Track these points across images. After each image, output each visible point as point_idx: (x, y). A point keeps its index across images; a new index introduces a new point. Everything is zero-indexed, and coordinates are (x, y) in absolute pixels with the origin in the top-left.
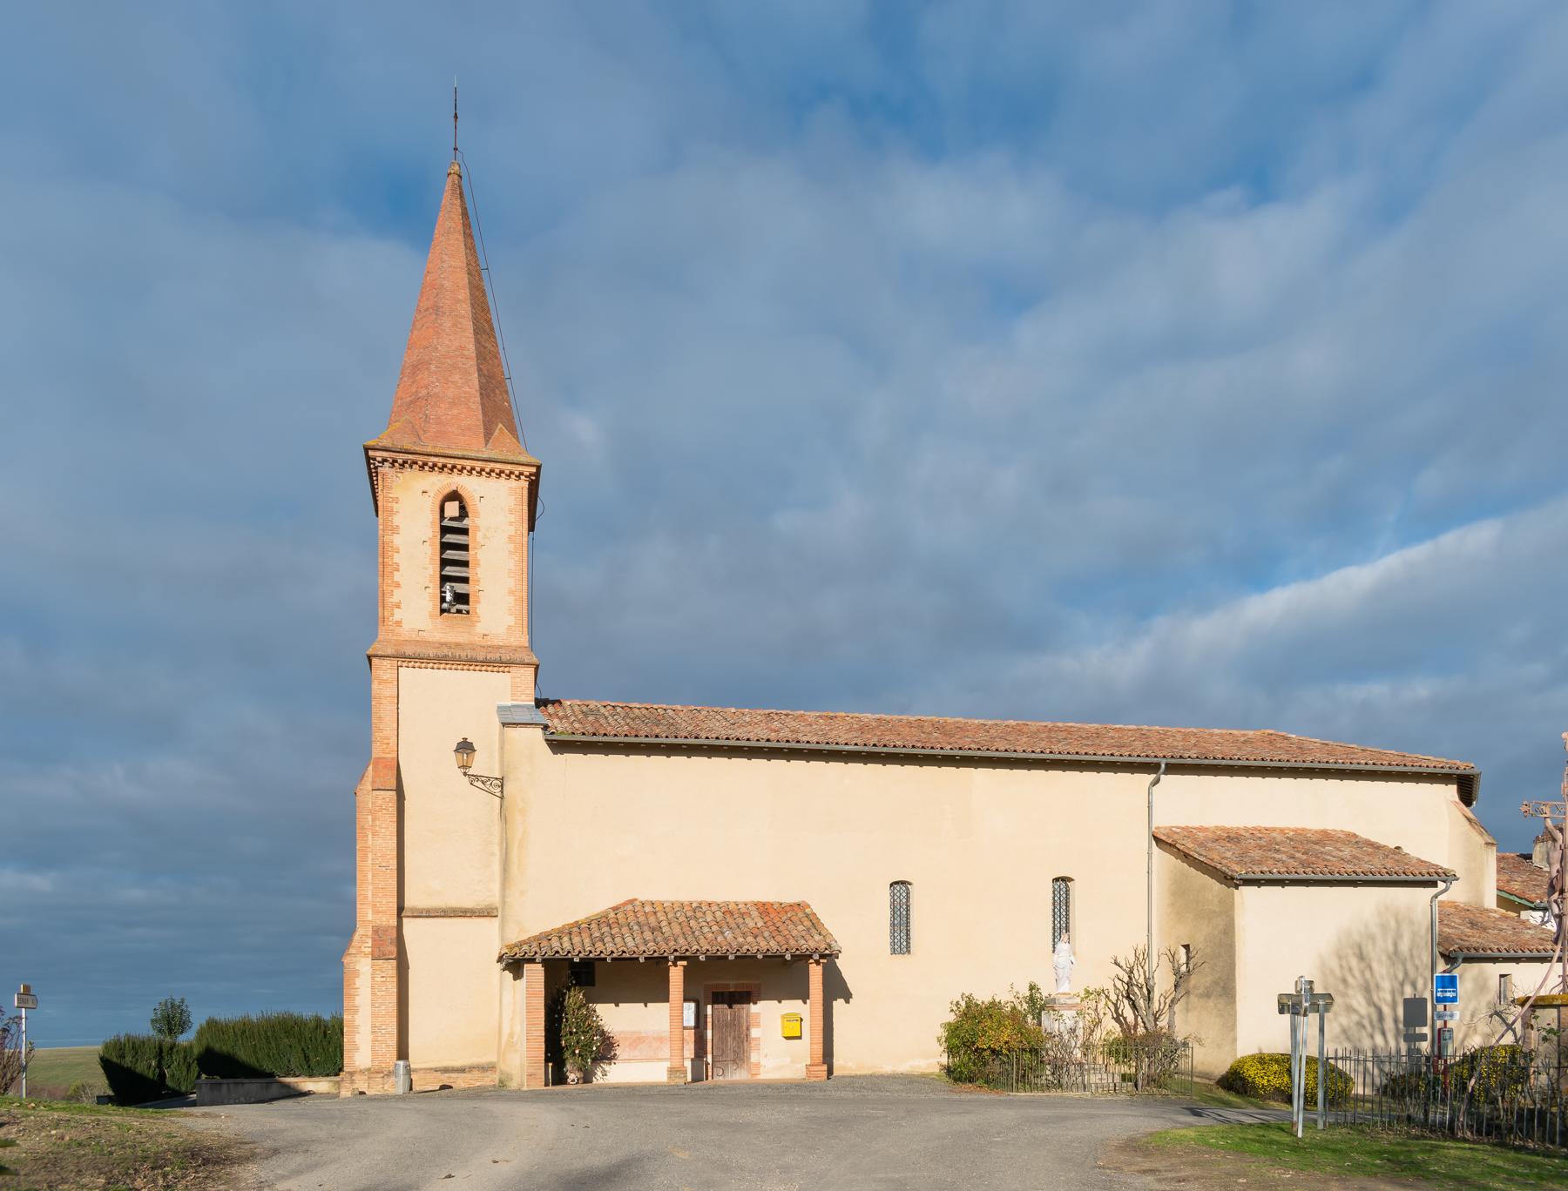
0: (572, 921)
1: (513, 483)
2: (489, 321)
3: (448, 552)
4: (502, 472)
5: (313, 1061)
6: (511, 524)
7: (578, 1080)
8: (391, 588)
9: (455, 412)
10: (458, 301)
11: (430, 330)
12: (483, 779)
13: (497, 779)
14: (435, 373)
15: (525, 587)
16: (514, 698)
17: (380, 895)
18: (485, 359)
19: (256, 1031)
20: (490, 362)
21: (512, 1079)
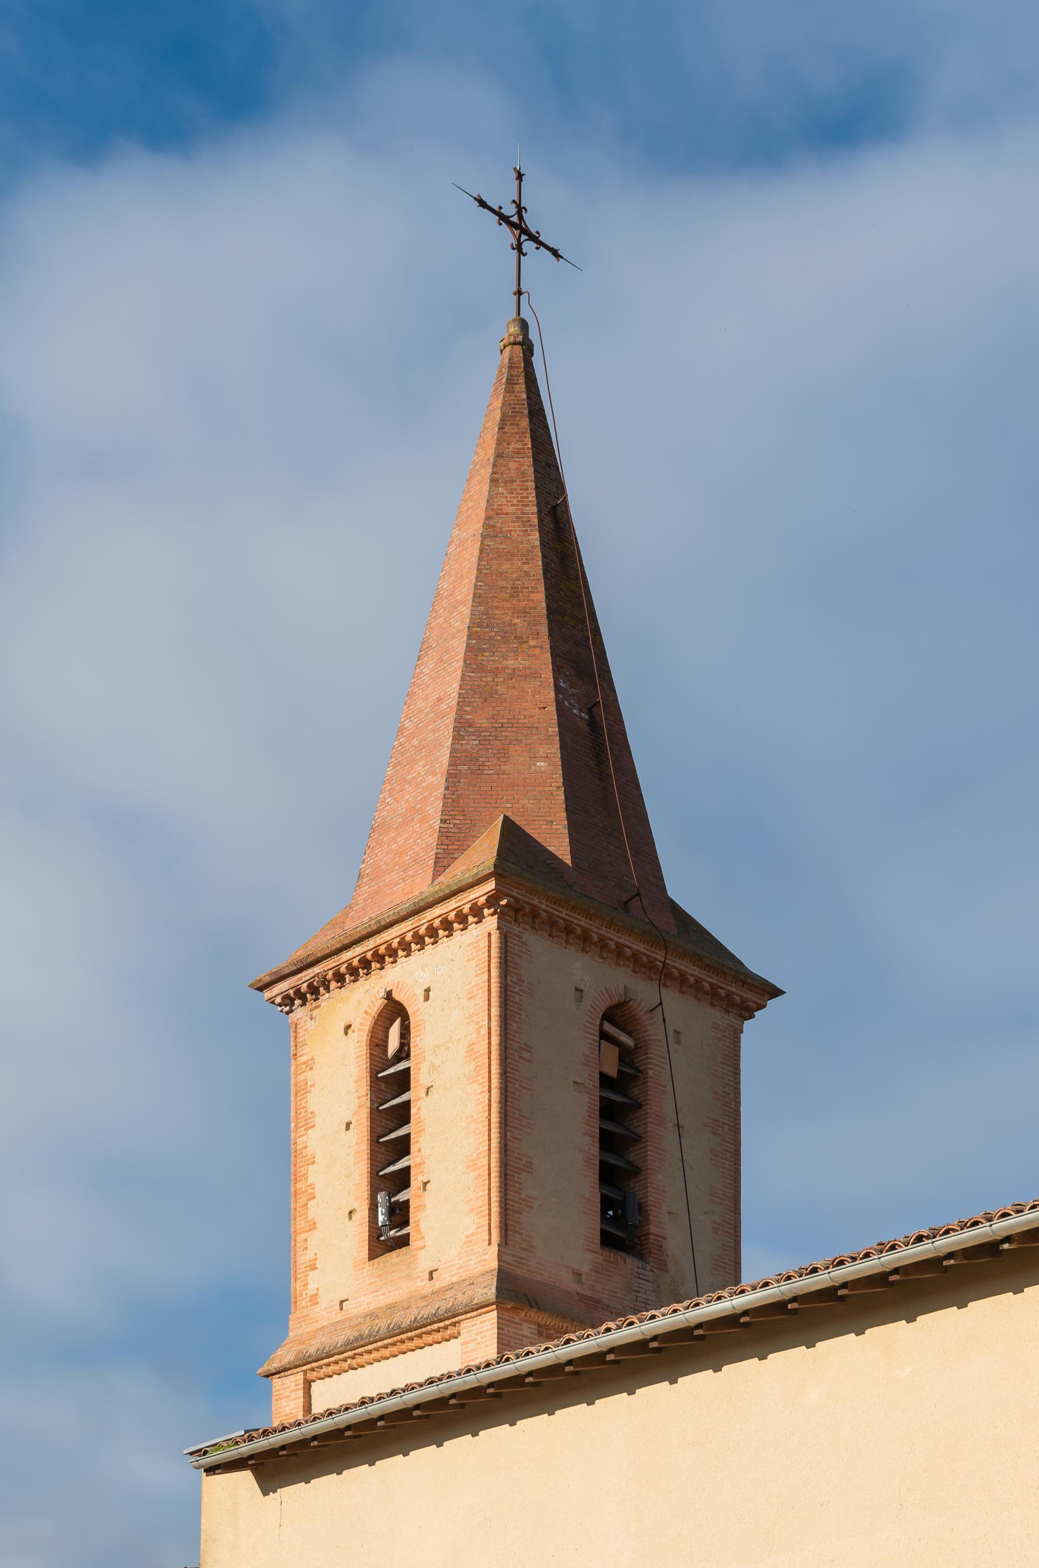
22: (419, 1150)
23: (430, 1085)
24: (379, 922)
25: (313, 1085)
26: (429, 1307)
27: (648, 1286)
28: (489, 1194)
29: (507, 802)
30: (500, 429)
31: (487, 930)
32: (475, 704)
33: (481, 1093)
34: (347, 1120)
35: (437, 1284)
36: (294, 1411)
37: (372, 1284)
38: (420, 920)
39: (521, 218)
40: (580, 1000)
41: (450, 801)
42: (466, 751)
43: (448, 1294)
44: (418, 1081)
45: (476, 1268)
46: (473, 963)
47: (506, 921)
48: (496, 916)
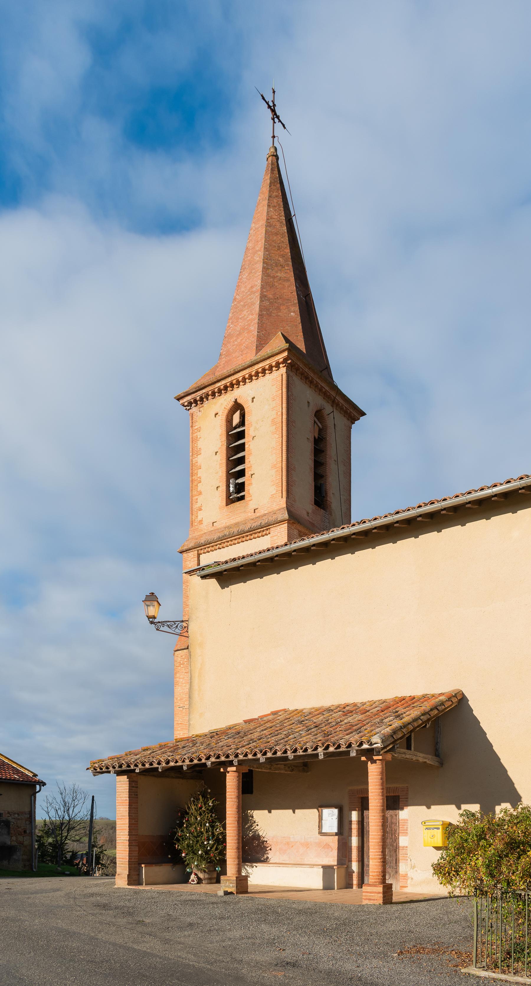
12: (168, 623)
17: (179, 729)
22: (250, 462)
23: (254, 436)
24: (235, 370)
25: (200, 438)
26: (256, 523)
27: (327, 520)
28: (282, 478)
29: (281, 327)
30: (270, 186)
31: (281, 373)
32: (267, 289)
33: (278, 438)
34: (216, 451)
35: (258, 514)
36: (193, 566)
37: (228, 515)
38: (252, 369)
39: (274, 108)
40: (309, 406)
41: (260, 324)
42: (265, 306)
43: (264, 518)
44: (249, 434)
45: (276, 507)
46: (275, 387)
47: (288, 370)
48: (286, 367)
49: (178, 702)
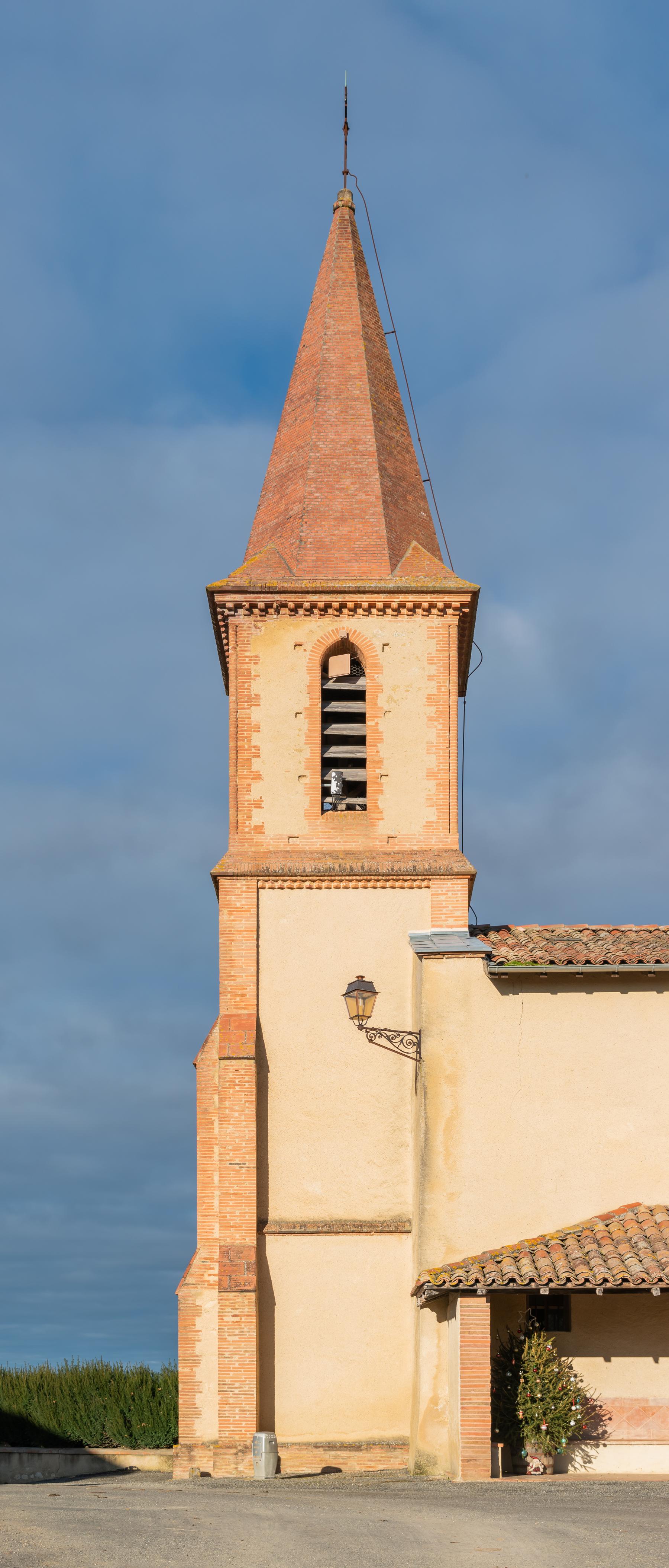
0: (535, 1235)
1: (434, 620)
2: (396, 403)
3: (334, 726)
4: (417, 606)
5: (136, 1428)
6: (431, 678)
7: (545, 1468)
8: (249, 781)
9: (344, 529)
10: (350, 378)
11: (308, 423)
12: (389, 1033)
13: (411, 1033)
14: (313, 480)
15: (453, 767)
16: (436, 923)
17: (231, 1203)
18: (390, 454)
19: (57, 1385)
20: (399, 457)
21: (435, 1464)
33: (442, 730)
49: (228, 1154)
